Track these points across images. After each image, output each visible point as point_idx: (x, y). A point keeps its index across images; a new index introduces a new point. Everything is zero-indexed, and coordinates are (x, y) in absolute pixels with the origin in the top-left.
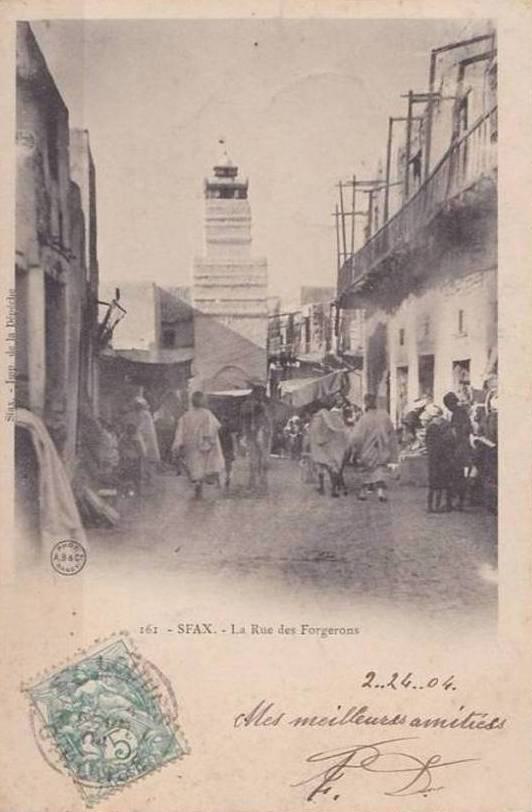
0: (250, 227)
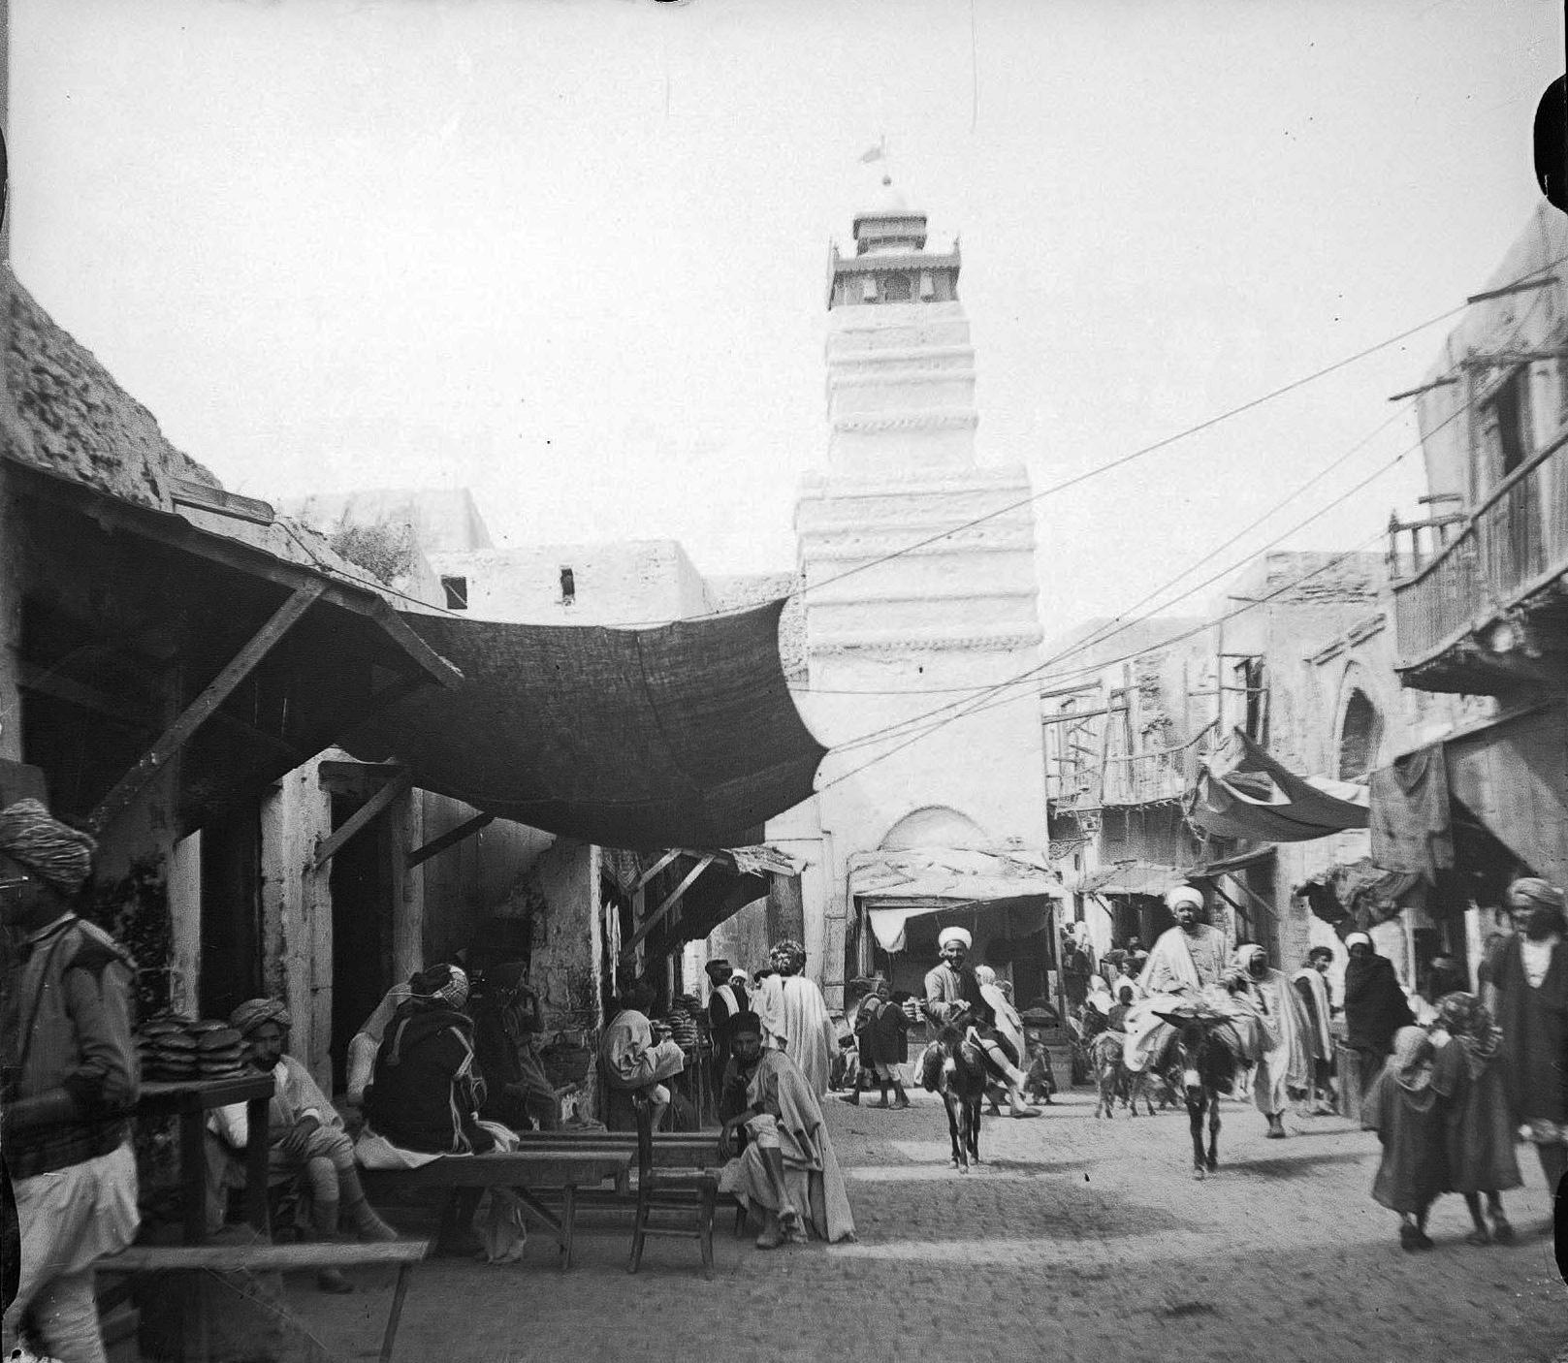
0: (972, 381)
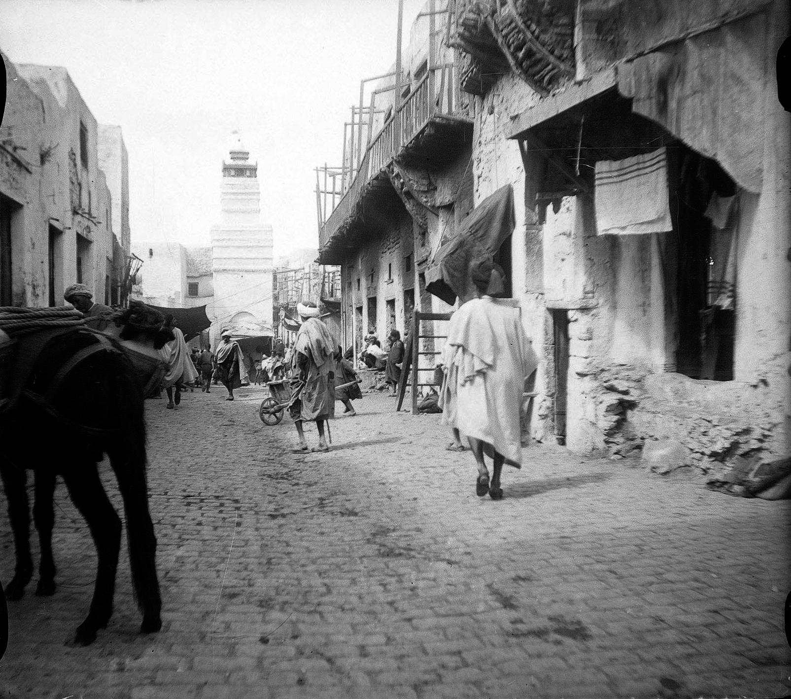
0: (259, 200)
